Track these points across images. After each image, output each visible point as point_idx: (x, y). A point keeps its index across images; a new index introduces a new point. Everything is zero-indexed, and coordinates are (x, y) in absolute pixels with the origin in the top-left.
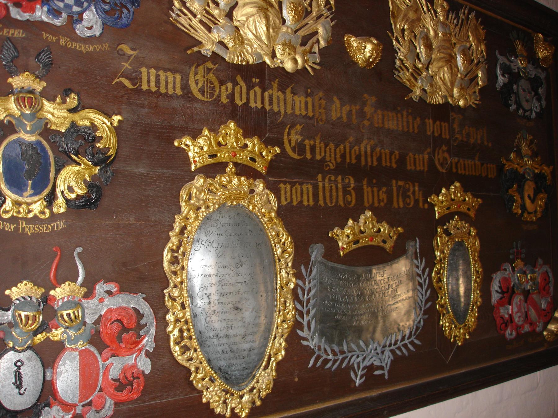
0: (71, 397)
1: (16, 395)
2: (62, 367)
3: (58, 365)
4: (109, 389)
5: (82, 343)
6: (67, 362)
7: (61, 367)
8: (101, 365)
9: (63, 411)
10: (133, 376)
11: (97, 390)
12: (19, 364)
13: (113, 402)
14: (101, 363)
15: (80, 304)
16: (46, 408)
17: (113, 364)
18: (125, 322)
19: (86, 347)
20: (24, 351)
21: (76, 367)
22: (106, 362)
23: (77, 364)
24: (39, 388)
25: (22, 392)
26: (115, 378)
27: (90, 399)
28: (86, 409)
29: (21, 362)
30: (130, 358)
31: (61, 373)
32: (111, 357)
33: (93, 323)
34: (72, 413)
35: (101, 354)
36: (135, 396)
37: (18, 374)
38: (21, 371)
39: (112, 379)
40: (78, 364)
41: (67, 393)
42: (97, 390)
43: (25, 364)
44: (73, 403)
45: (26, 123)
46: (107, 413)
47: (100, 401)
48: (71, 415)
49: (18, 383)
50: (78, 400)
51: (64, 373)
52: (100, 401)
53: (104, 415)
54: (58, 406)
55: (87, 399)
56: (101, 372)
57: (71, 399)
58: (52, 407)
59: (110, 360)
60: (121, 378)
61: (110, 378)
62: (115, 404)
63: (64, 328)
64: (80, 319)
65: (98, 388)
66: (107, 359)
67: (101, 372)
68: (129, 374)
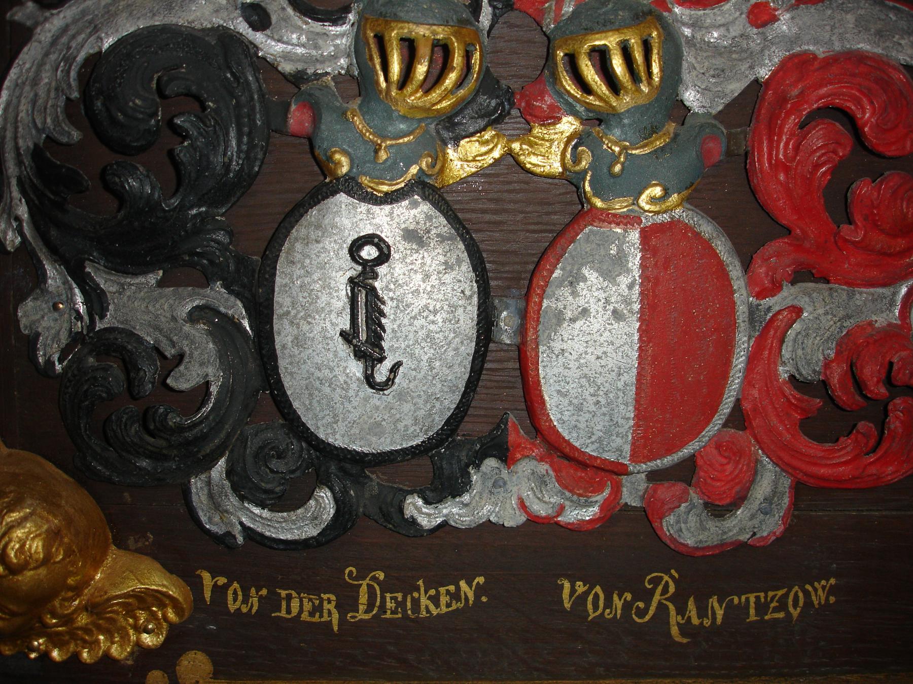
0: (599, 426)
1: (354, 386)
2: (566, 291)
3: (547, 284)
4: (774, 421)
5: (657, 191)
6: (586, 271)
7: (559, 292)
8: (742, 310)
9: (565, 487)
10: (889, 381)
11: (718, 421)
12: (369, 252)
13: (786, 482)
14: (742, 298)
15: (660, 19)
16: (491, 463)
17: (797, 311)
18: (867, 115)
19: (678, 212)
20: (390, 198)
21: (627, 302)
22: (767, 302)
23: (631, 287)
24: (456, 369)
25: (381, 373)
26: (807, 373)
27: (686, 451)
28: (666, 492)
29: (377, 246)
30: (882, 297)
31: (559, 317)
32: (793, 283)
33: (716, 117)
34: (600, 498)
35: (747, 265)
36: (890, 469)
37: (362, 298)
38: (377, 284)
39: (792, 377)
40: (637, 289)
41: (579, 409)
42: (718, 421)
43: (395, 255)
44: (606, 456)
45: (824, 660)
46: (756, 522)
47: (729, 468)
48: (596, 509)
49: (363, 336)
50: (627, 448)
51: (573, 320)
52: (729, 468)
53: (742, 530)
54: (541, 459)
55: (669, 451)
56: (743, 344)
57: (600, 440)
58: (515, 461)
59: (787, 296)
60: (835, 380)
61: (783, 372)
62: (798, 489)
63: (583, 121)
64: (656, 79)
65: (726, 407)
66: (775, 288)
67: (743, 344)
68: (871, 372)
